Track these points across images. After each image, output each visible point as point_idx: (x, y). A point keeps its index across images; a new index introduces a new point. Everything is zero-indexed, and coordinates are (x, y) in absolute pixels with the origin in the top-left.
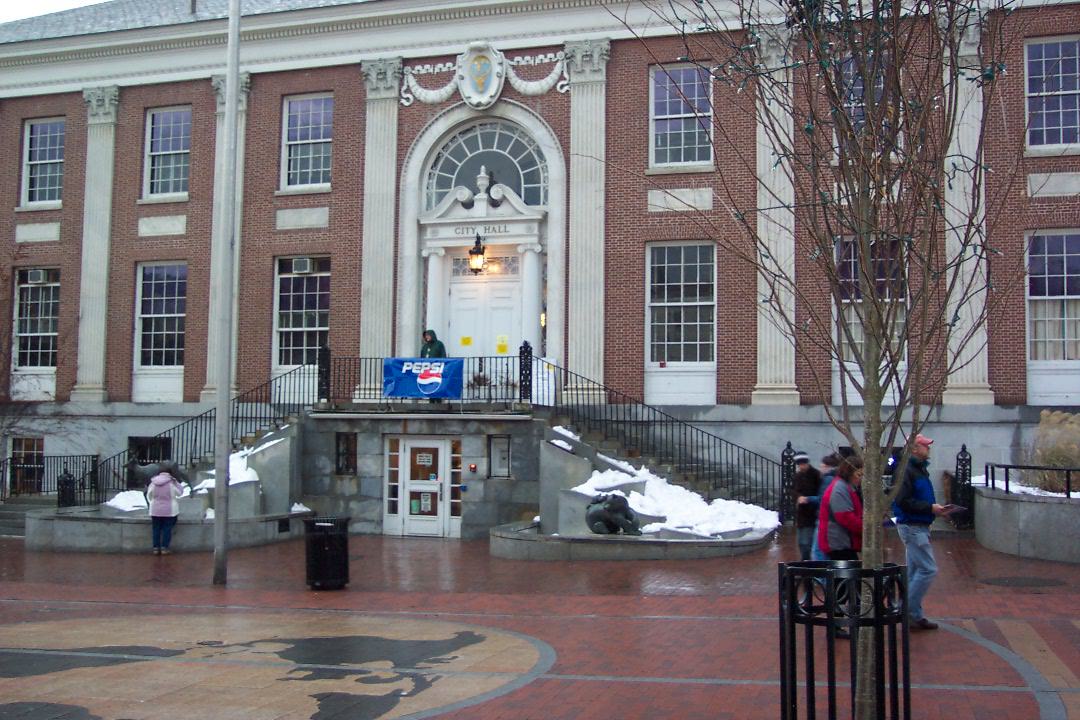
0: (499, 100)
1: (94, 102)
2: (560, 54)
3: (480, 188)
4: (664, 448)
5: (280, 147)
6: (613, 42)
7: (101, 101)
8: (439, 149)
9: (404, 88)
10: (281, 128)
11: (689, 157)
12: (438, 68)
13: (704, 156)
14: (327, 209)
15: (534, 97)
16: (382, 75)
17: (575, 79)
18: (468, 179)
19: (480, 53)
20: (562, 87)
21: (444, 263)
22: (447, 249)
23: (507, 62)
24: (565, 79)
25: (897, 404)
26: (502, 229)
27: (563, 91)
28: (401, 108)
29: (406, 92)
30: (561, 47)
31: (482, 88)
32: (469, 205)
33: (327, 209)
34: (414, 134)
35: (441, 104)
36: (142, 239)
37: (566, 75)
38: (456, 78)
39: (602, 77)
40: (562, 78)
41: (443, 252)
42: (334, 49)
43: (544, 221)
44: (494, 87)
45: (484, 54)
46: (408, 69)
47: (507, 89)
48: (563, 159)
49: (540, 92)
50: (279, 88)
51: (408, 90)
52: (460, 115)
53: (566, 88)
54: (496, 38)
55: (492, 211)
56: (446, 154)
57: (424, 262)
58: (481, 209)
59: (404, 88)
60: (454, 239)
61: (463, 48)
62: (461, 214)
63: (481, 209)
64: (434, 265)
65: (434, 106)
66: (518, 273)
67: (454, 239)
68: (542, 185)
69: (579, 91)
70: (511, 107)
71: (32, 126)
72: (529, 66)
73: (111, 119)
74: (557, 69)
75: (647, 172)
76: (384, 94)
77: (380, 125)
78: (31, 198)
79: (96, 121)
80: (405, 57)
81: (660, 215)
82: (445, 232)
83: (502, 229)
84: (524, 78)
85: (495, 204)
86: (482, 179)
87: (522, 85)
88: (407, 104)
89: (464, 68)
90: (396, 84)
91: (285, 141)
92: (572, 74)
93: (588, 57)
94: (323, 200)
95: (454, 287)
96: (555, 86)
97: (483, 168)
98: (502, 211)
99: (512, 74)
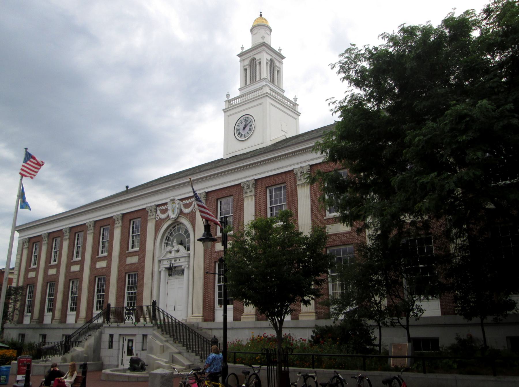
1: (149, 211)
5: (267, 208)
7: (151, 211)
12: (162, 207)
15: (187, 214)
19: (173, 201)
23: (182, 203)
28: (156, 221)
42: (270, 169)
44: (177, 212)
46: (158, 208)
47: (181, 213)
51: (158, 215)
52: (169, 223)
54: (176, 196)
57: (160, 272)
61: (168, 200)
71: (221, 202)
72: (187, 204)
73: (253, 193)
76: (249, 194)
77: (151, 226)
89: (169, 206)
94: (137, 253)
95: (169, 281)
99: (182, 206)
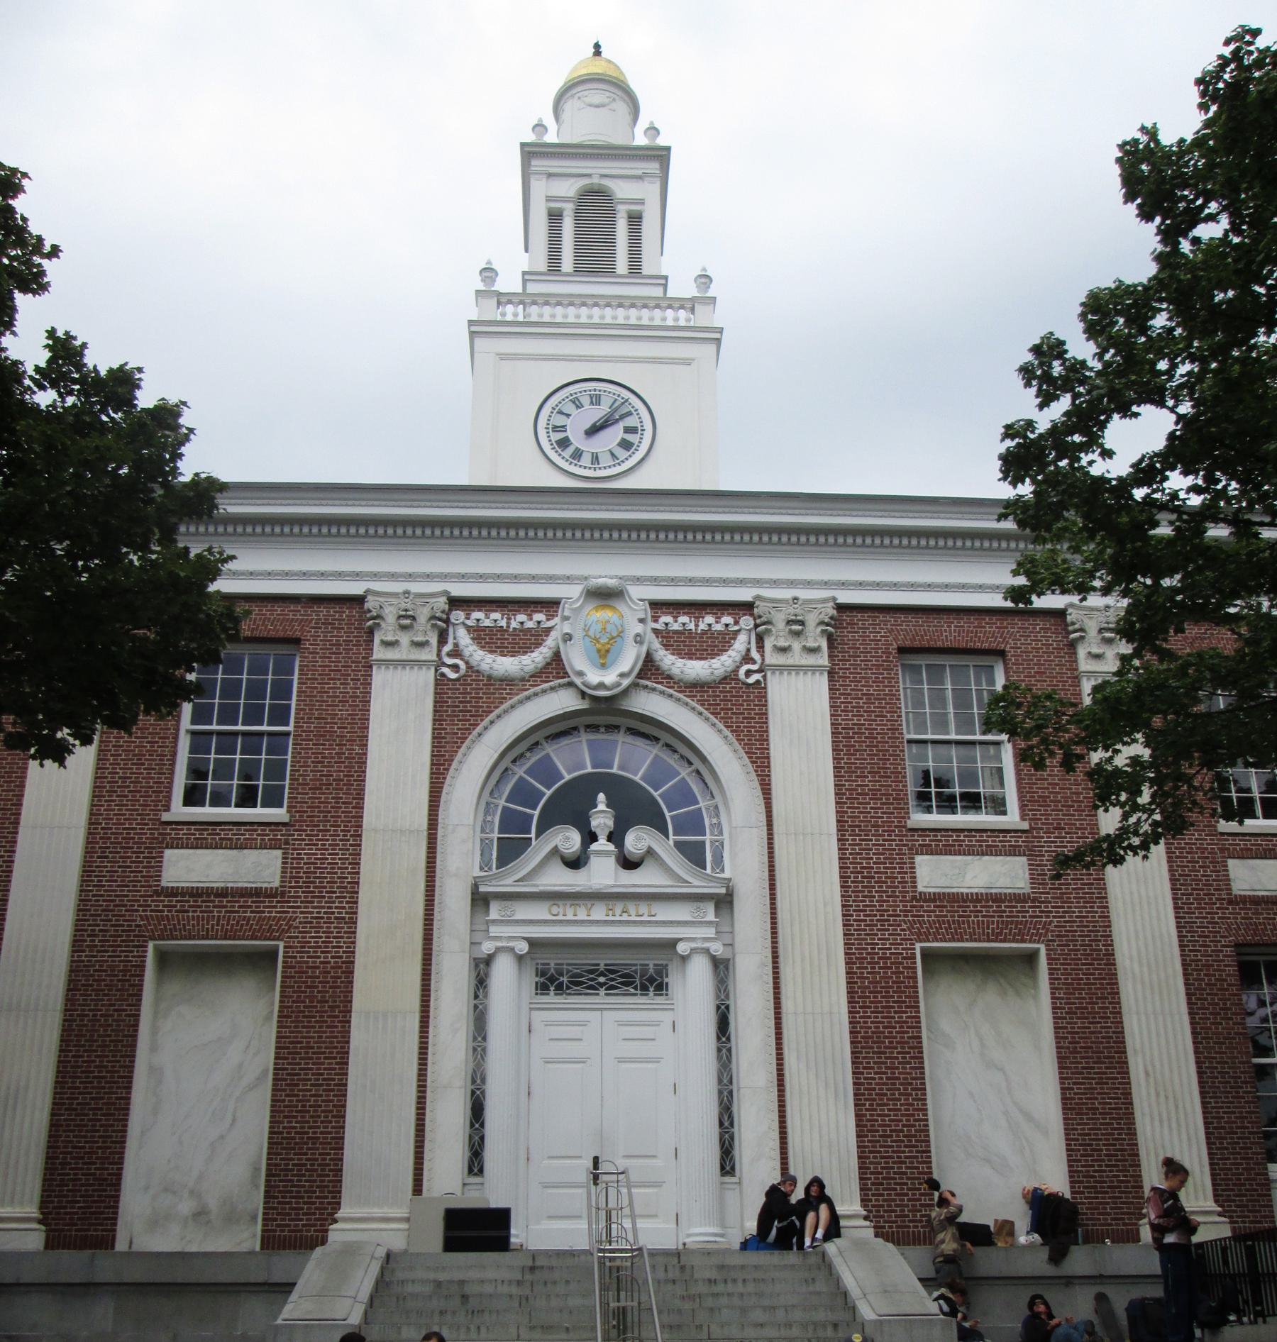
0: (634, 685)
2: (747, 622)
3: (598, 832)
4: (821, 1316)
6: (841, 608)
9: (447, 648)
11: (247, 799)
13: (273, 799)
16: (796, 625)
17: (772, 658)
20: (748, 673)
21: (520, 969)
22: (533, 943)
24: (754, 662)
25: (43, 1228)
27: (751, 680)
28: (441, 680)
29: (449, 655)
30: (746, 607)
31: (604, 656)
32: (575, 863)
36: (173, 892)
37: (755, 654)
39: (823, 659)
40: (747, 659)
41: (523, 947)
43: (724, 902)
44: (628, 659)
46: (458, 616)
47: (649, 669)
48: (756, 784)
49: (710, 678)
51: (456, 653)
52: (561, 702)
62: (559, 879)
64: (504, 974)
65: (508, 682)
68: (708, 838)
74: (740, 644)
75: (166, 817)
77: (399, 708)
78: (192, 797)
79: (391, 654)
80: (453, 594)
84: (679, 653)
85: (629, 864)
86: (602, 819)
87: (669, 661)
88: (453, 675)
90: (434, 641)
93: (796, 625)
96: (736, 671)
97: (601, 797)
99: (656, 644)
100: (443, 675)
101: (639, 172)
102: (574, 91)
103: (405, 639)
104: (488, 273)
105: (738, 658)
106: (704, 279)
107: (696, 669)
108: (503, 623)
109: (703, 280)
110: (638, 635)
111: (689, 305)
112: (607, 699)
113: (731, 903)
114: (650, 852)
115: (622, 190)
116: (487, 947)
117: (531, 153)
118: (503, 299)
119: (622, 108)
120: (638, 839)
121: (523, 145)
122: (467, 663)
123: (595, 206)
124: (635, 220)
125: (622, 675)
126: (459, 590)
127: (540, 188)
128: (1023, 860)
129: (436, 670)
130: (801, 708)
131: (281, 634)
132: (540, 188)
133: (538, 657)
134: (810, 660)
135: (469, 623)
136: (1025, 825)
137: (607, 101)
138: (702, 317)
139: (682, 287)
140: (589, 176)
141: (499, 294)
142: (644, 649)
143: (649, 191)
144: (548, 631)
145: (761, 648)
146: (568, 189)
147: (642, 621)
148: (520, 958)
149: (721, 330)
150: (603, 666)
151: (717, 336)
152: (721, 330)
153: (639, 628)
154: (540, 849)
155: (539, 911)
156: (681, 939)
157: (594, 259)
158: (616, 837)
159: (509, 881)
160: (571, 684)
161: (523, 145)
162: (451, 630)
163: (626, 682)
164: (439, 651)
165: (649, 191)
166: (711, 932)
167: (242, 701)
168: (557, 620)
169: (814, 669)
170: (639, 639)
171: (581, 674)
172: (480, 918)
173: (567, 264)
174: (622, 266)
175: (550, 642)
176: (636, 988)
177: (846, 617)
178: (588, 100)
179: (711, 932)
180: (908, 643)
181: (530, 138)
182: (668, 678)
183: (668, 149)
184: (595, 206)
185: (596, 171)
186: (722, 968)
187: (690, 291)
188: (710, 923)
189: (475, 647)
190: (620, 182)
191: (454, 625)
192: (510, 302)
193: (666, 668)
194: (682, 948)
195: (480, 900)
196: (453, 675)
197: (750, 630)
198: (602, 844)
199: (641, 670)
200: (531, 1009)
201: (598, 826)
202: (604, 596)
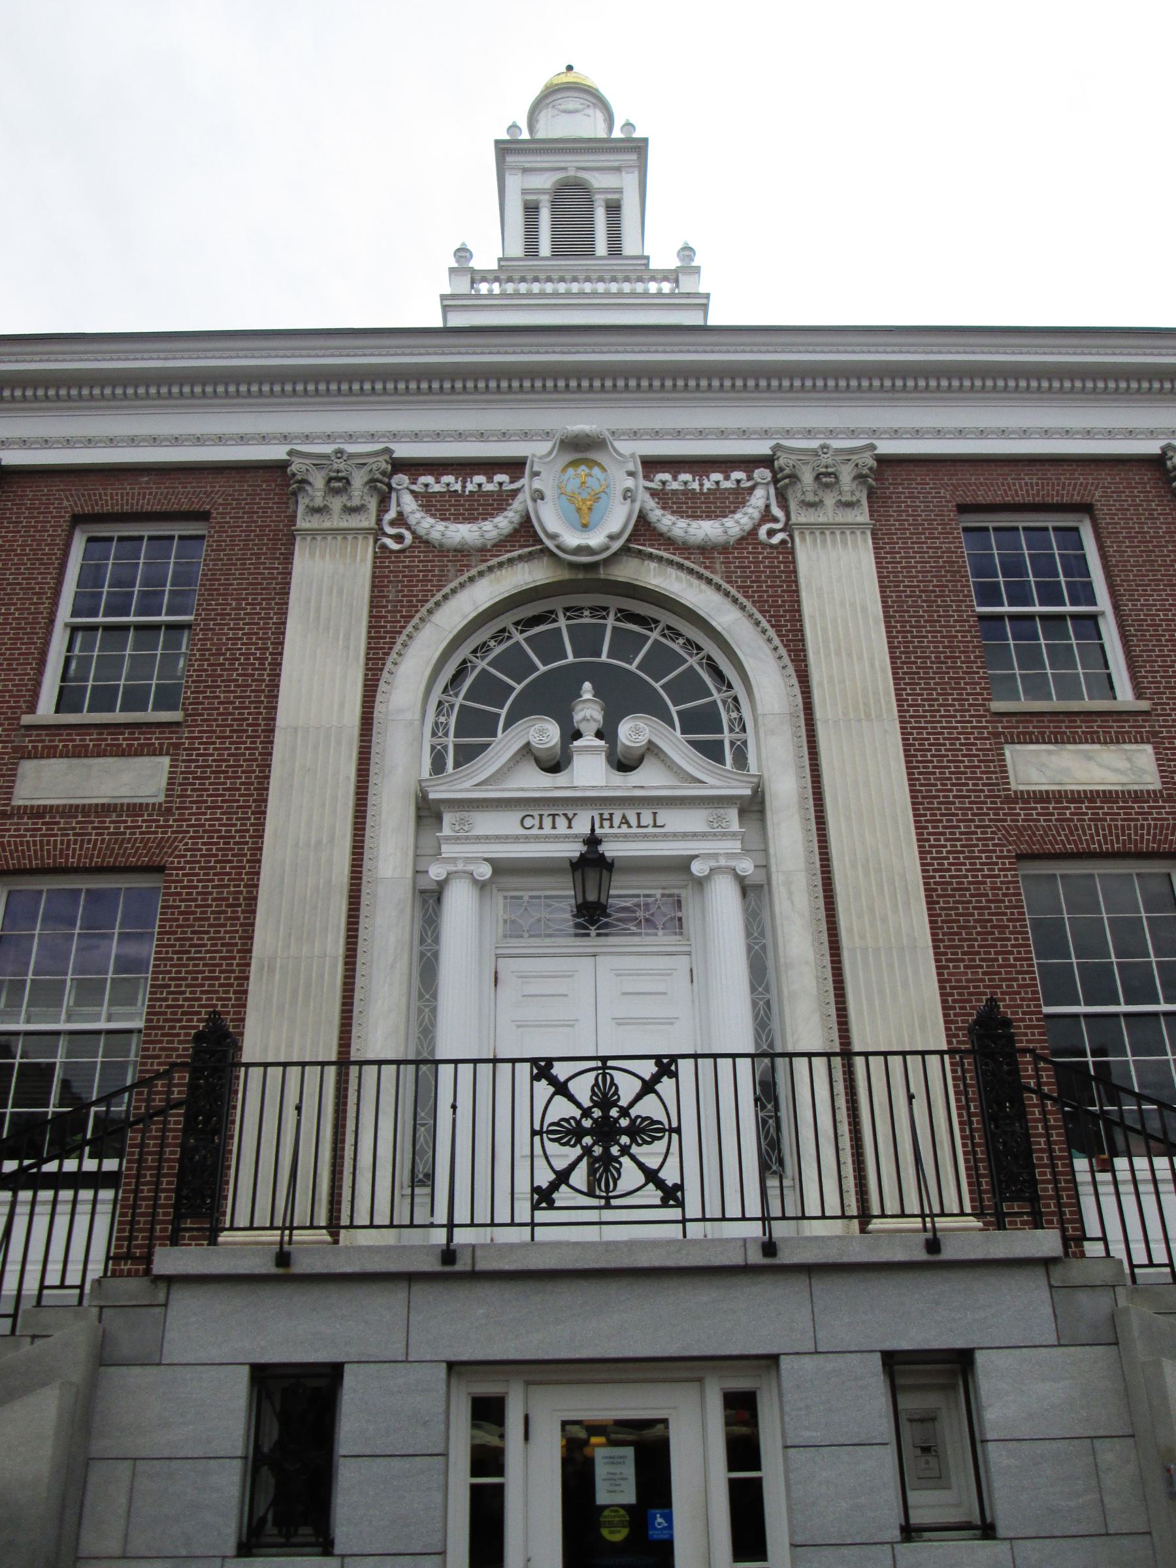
0: (625, 550)
3: (583, 727)
5: (51, 621)
6: (885, 461)
8: (464, 652)
9: (392, 514)
10: (60, 582)
14: (166, 761)
16: (338, 484)
18: (553, 698)
20: (771, 533)
26: (647, 819)
27: (776, 540)
29: (392, 523)
32: (555, 765)
33: (166, 761)
34: (411, 605)
35: (483, 551)
37: (777, 511)
38: (524, 497)
39: (862, 515)
40: (767, 516)
41: (486, 871)
43: (753, 807)
44: (616, 519)
45: (593, 455)
46: (401, 480)
47: (643, 528)
50: (70, 500)
51: (400, 520)
53: (780, 537)
55: (618, 779)
56: (482, 664)
57: (430, 900)
58: (589, 772)
59: (392, 514)
60: (516, 839)
63: (589, 772)
64: (460, 905)
65: (462, 556)
66: (565, 91)
67: (516, 839)
69: (815, 541)
70: (653, 565)
74: (758, 499)
77: (328, 585)
79: (315, 522)
81: (1043, 797)
82: (487, 823)
83: (647, 819)
84: (679, 513)
85: (624, 764)
87: (666, 521)
88: (395, 546)
90: (373, 505)
91: (64, 614)
92: (793, 506)
97: (587, 685)
98: (648, 779)
99: (651, 503)
100: (384, 547)
101: (617, 164)
102: (548, 101)
103: (336, 503)
104: (463, 253)
105: (756, 515)
106: (687, 252)
107: (706, 530)
108: (458, 487)
109: (687, 253)
110: (628, 490)
111: (672, 276)
112: (593, 566)
113: (762, 812)
114: (651, 748)
115: (598, 181)
116: (436, 872)
117: (505, 150)
118: (477, 277)
119: (600, 116)
120: (637, 731)
121: (497, 142)
122: (413, 533)
123: (572, 199)
124: (614, 209)
125: (612, 537)
126: (403, 451)
127: (514, 183)
128: (1149, 748)
129: (376, 541)
130: (841, 579)
131: (185, 507)
132: (514, 183)
133: (503, 523)
134: (850, 516)
135: (414, 487)
136: (1144, 705)
137: (581, 107)
138: (686, 285)
139: (663, 258)
140: (565, 169)
141: (473, 271)
142: (637, 506)
143: (629, 182)
144: (514, 493)
145: (784, 505)
146: (545, 181)
147: (631, 474)
148: (482, 886)
149: (707, 296)
150: (585, 527)
151: (704, 301)
152: (707, 296)
153: (630, 483)
154: (505, 744)
155: (507, 823)
156: (696, 856)
157: (573, 241)
158: (606, 733)
159: (468, 784)
160: (546, 551)
161: (497, 142)
162: (394, 495)
163: (616, 545)
164: (379, 521)
165: (629, 182)
166: (735, 846)
167: (159, 652)
168: (524, 481)
169: (853, 527)
170: (628, 495)
171: (553, 537)
172: (427, 841)
173: (545, 249)
174: (601, 248)
175: (517, 504)
176: (639, 925)
177: (888, 473)
178: (563, 107)
179: (735, 846)
180: (969, 500)
181: (505, 136)
182: (667, 541)
183: (645, 140)
184: (572, 199)
185: (572, 165)
186: (754, 893)
187: (673, 263)
188: (734, 834)
189: (423, 514)
190: (597, 174)
191: (397, 491)
192: (484, 280)
193: (664, 529)
194: (697, 868)
195: (428, 812)
196: (395, 546)
197: (767, 484)
198: (589, 740)
199: (631, 535)
200: (498, 956)
201: (585, 719)
202: (581, 449)
